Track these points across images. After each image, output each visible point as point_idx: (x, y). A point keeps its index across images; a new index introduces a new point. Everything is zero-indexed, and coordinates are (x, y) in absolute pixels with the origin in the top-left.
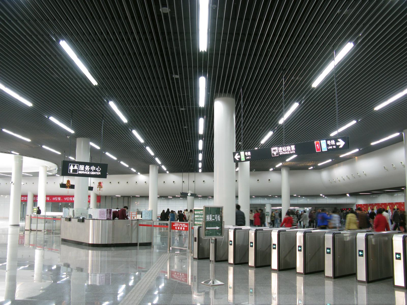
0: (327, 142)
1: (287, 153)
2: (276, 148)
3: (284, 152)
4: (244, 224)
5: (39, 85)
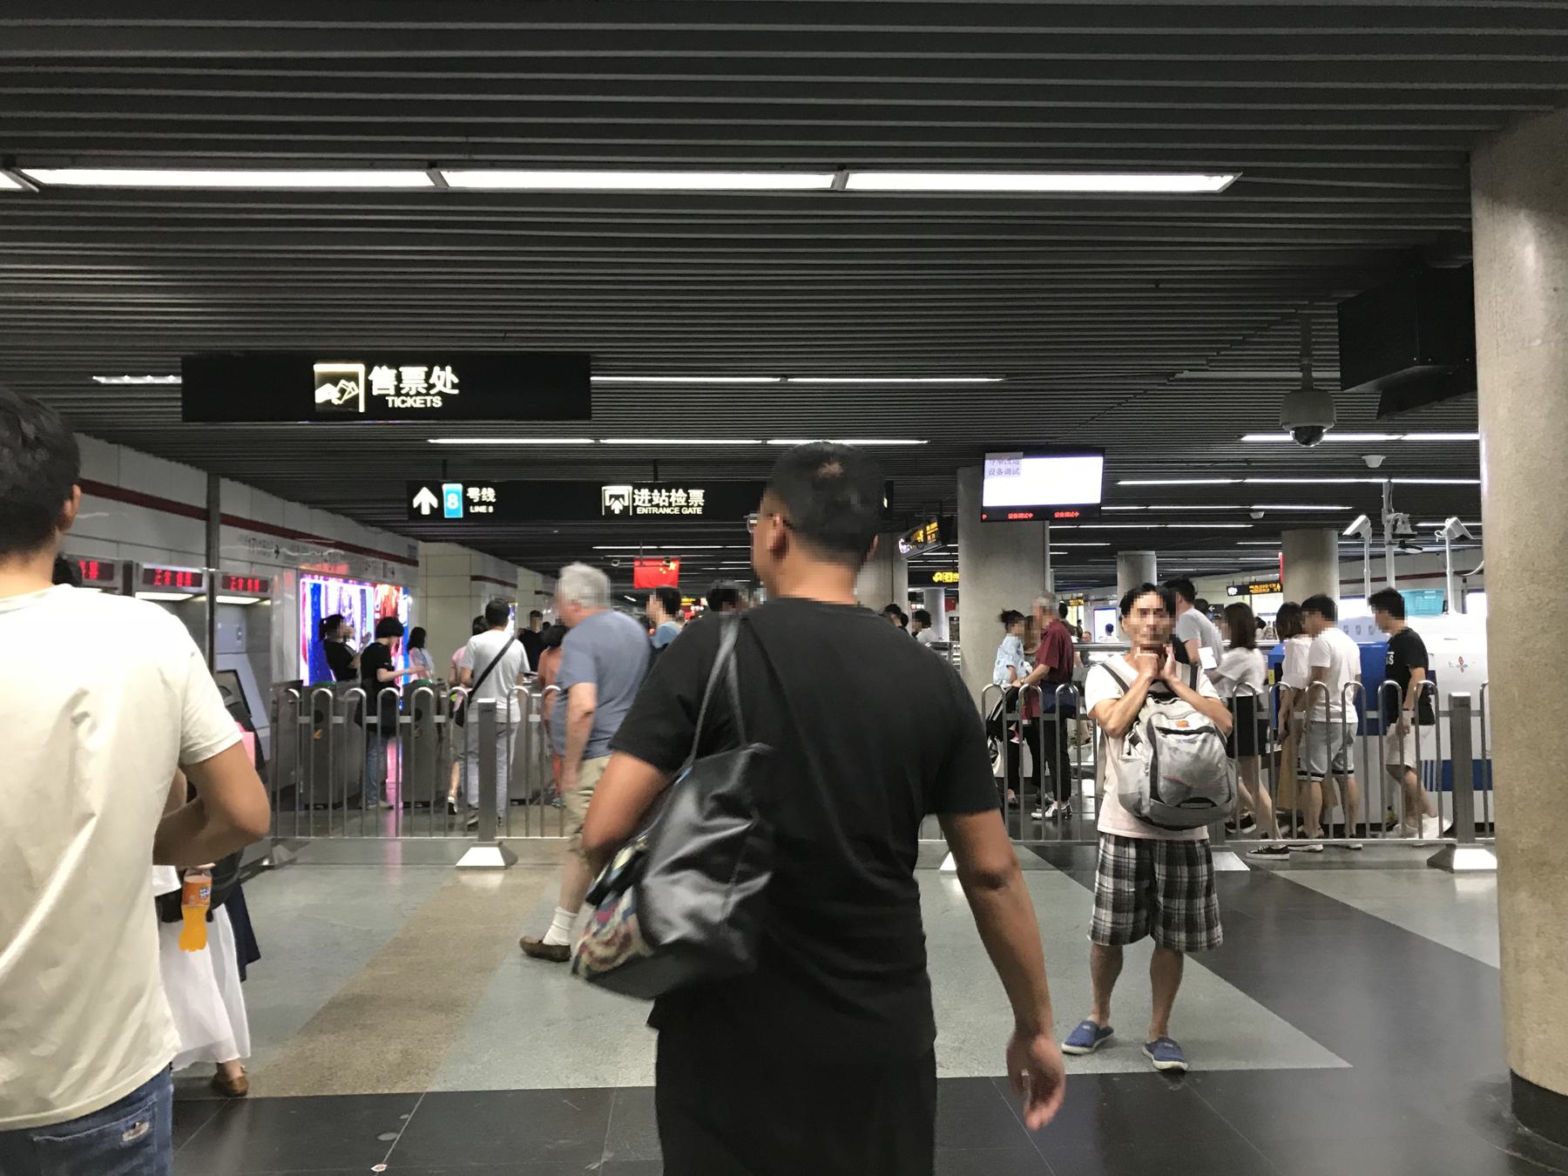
0: (465, 492)
1: (668, 511)
2: (625, 490)
3: (658, 506)
4: (911, 583)
5: (1097, 290)
